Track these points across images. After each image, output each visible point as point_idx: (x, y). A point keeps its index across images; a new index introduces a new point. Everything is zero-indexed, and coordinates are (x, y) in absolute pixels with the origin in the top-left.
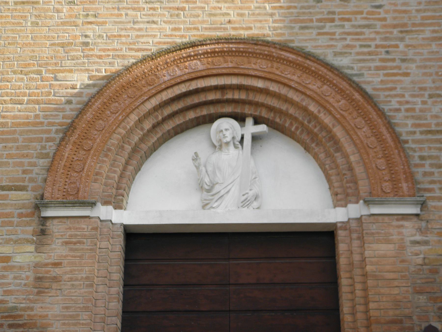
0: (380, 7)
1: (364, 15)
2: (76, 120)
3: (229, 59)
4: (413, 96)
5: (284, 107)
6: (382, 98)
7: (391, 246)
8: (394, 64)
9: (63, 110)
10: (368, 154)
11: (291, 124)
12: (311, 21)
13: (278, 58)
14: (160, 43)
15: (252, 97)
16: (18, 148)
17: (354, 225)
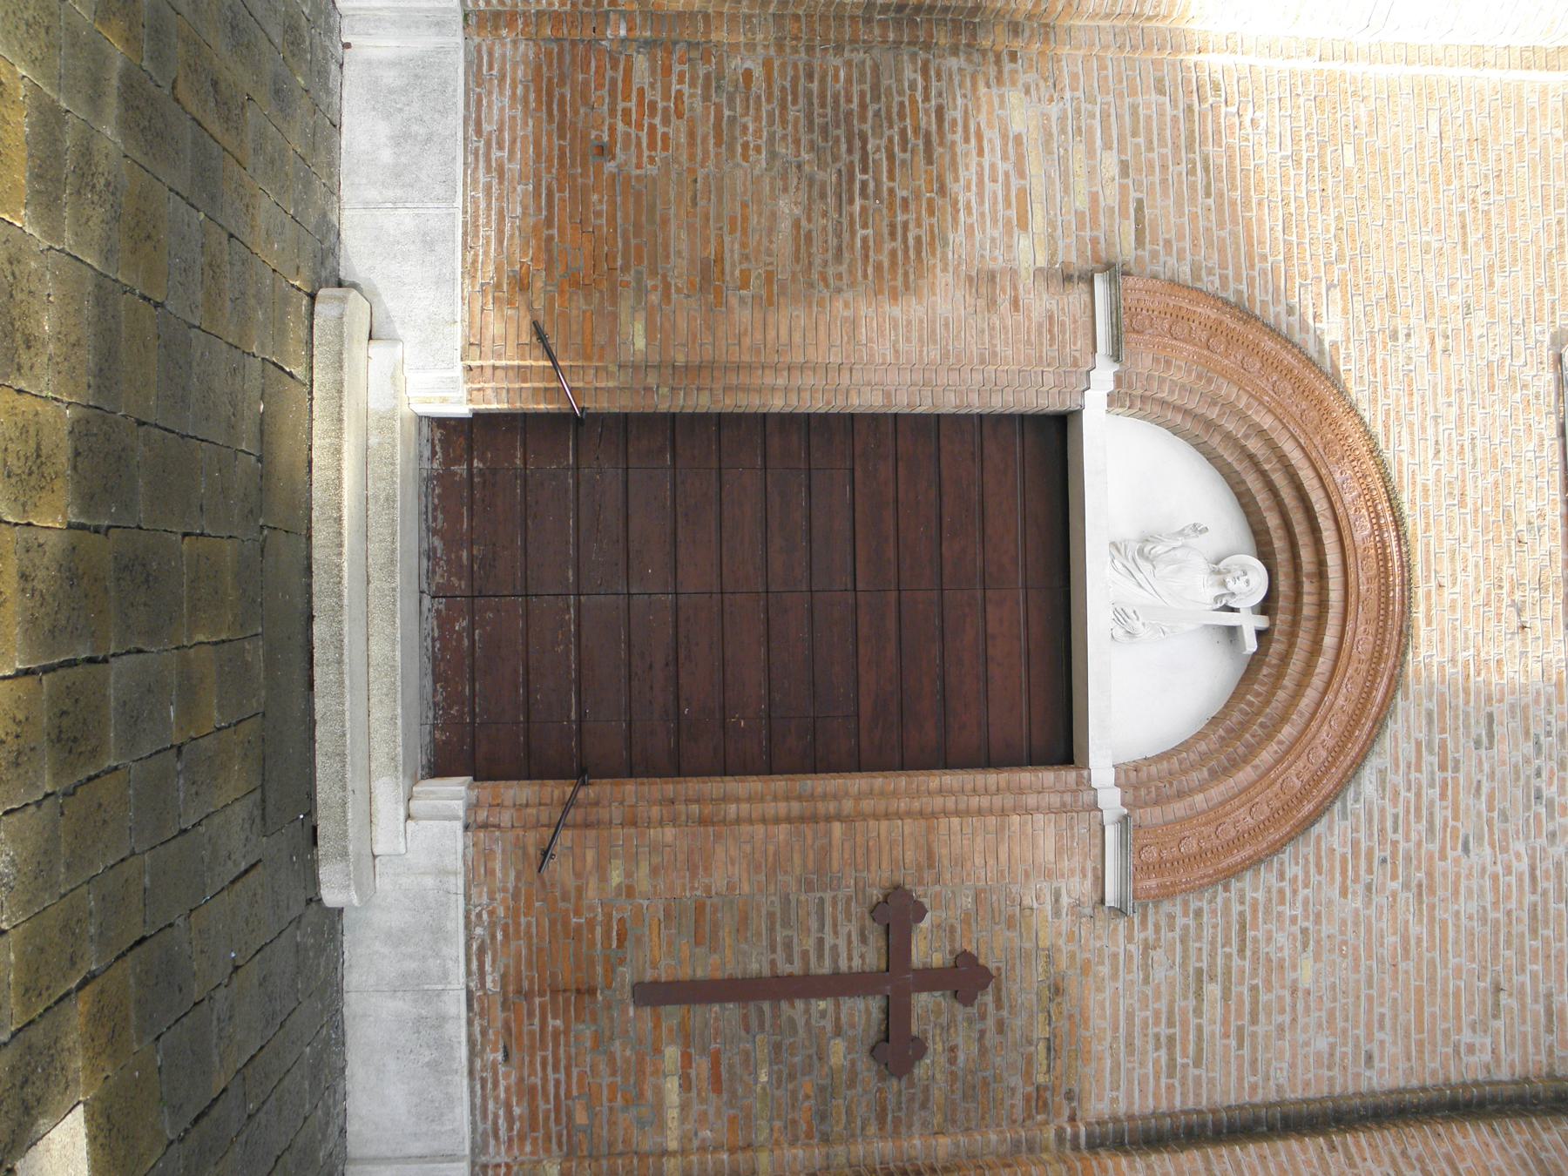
0: (1466, 849)
1: (1451, 823)
2: (1259, 324)
3: (1375, 586)
4: (1306, 902)
5: (1288, 682)
6: (1302, 850)
7: (1051, 857)
8: (1362, 873)
9: (1276, 301)
10: (1206, 824)
11: (1258, 694)
12: (1443, 731)
13: (1376, 671)
14: (1400, 464)
15: (1306, 626)
16: (1208, 229)
17: (1086, 797)
